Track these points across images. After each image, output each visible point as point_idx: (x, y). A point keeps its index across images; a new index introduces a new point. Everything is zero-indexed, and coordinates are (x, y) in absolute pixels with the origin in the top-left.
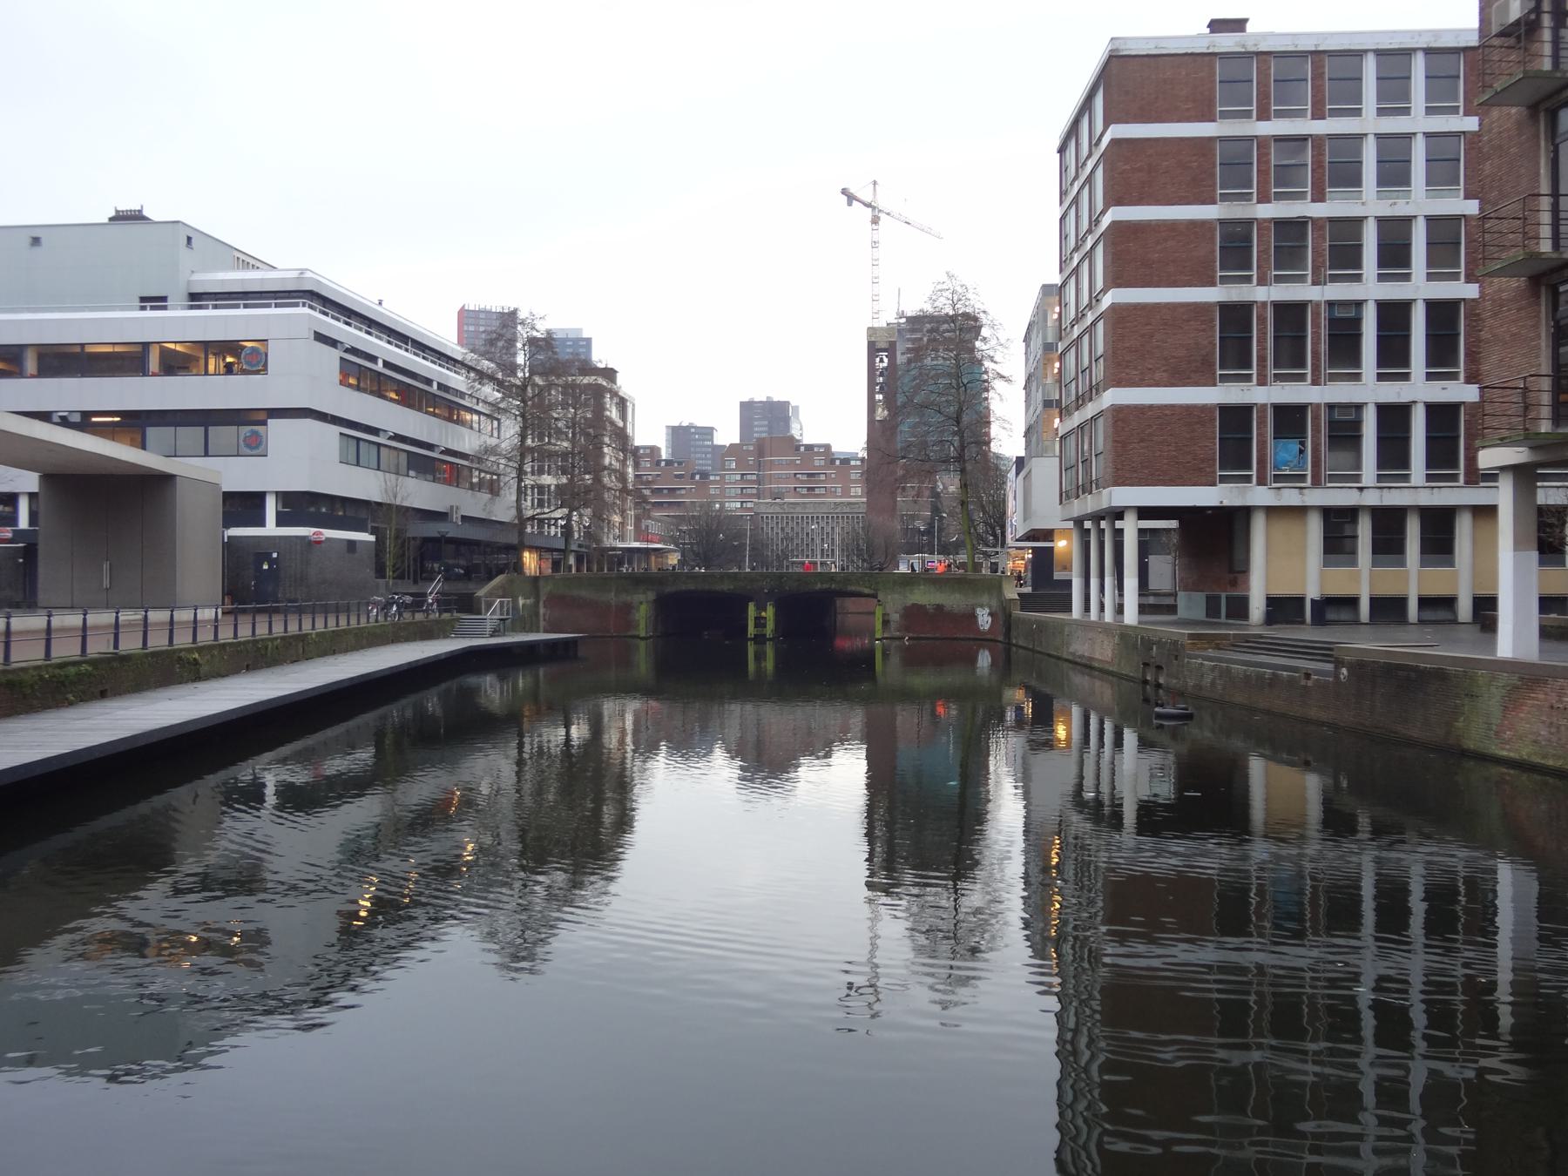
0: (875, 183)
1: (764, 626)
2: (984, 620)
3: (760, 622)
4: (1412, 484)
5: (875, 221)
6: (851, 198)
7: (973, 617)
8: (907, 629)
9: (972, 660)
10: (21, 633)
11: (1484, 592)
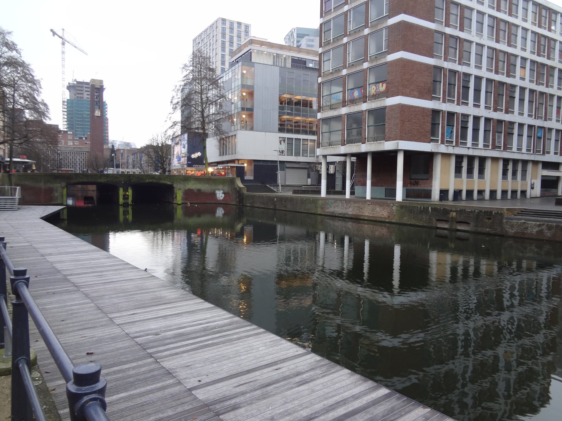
0: (63, 30)
1: (128, 198)
2: (220, 195)
3: (126, 197)
4: (468, 146)
5: (63, 44)
6: (54, 34)
7: (214, 194)
8: (186, 199)
9: (214, 212)
10: (110, 403)
11: (493, 189)
